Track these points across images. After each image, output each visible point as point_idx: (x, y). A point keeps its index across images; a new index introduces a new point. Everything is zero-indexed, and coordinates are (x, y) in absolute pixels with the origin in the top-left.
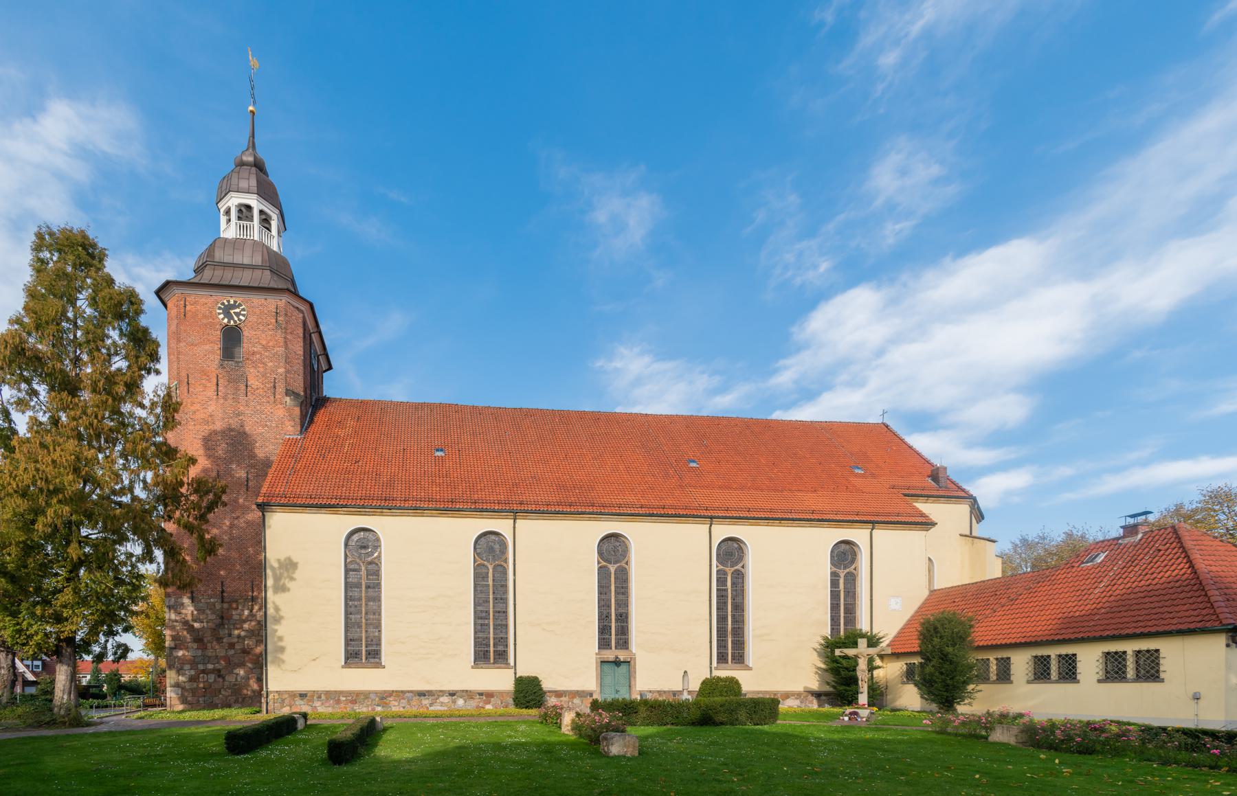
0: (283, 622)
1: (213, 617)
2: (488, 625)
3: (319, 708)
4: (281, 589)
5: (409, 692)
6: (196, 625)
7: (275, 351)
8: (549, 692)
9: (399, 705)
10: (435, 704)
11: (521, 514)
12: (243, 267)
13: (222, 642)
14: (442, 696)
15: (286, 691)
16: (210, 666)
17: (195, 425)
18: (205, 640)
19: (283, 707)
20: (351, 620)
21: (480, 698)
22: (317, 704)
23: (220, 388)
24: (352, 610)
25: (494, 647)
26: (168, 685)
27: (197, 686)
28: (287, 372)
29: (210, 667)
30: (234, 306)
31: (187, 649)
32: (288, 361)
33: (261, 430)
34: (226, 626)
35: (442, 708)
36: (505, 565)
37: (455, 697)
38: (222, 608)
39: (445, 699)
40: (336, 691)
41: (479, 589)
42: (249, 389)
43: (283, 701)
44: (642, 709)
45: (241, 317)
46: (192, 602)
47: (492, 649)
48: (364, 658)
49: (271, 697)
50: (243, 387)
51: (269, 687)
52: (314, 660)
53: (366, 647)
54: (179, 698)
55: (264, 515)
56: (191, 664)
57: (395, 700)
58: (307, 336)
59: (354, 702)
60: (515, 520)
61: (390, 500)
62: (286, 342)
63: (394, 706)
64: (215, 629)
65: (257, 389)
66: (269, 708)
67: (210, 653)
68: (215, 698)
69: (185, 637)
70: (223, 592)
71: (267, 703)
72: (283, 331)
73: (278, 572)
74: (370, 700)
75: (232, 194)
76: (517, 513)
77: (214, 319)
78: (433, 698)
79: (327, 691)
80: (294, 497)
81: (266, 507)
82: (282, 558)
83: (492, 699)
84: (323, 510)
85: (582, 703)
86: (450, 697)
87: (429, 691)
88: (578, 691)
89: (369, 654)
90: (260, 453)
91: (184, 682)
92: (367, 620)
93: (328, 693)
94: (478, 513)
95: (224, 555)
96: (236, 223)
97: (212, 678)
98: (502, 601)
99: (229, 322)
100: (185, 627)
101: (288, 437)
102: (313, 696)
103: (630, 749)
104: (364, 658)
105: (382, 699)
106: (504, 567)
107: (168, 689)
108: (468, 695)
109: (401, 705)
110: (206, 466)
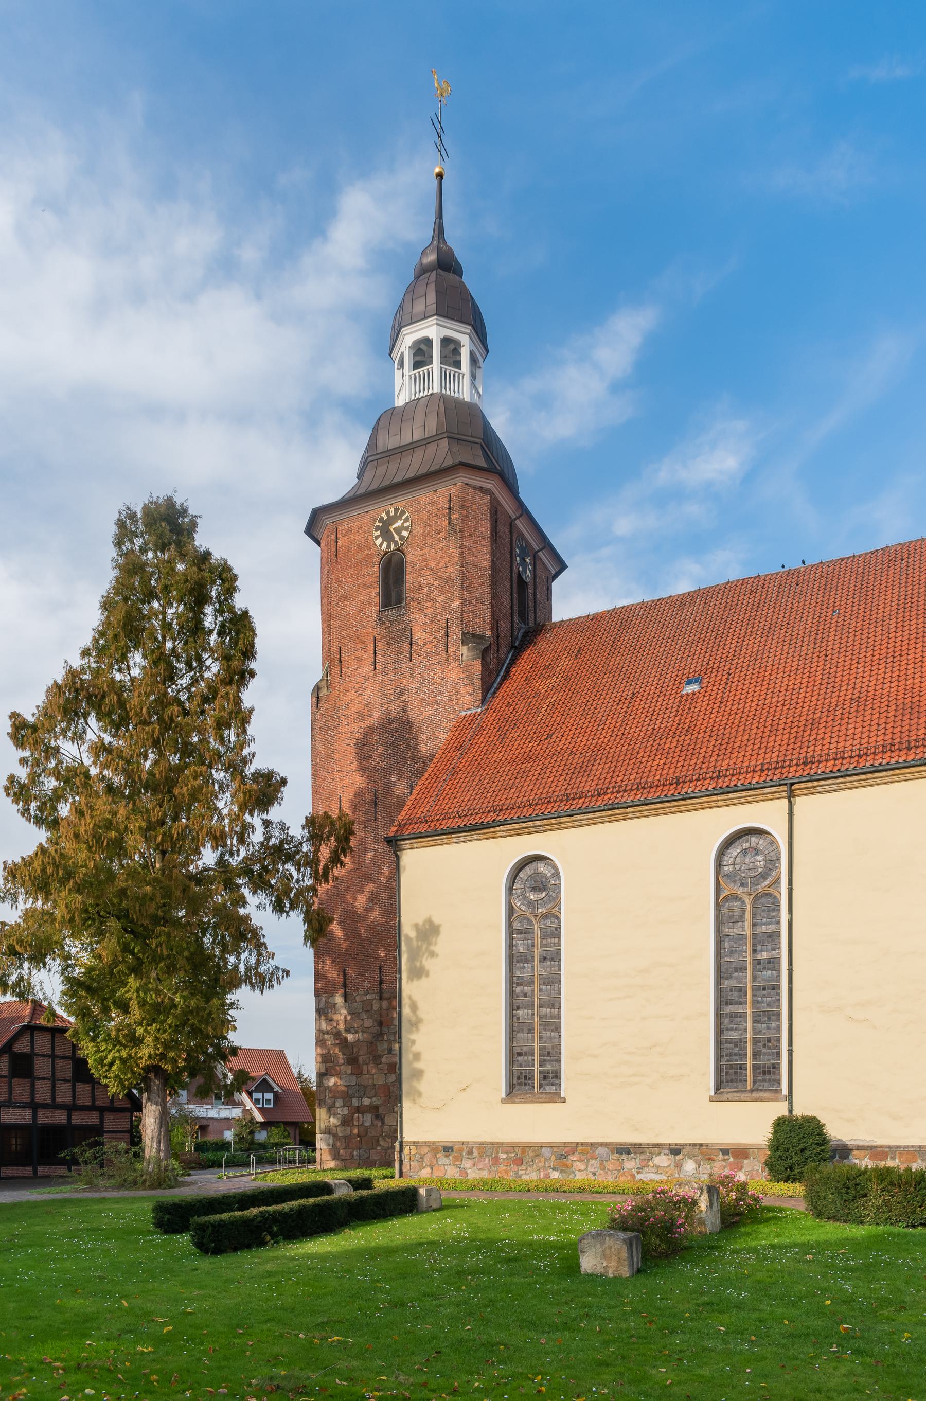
0: (422, 1028)
1: (368, 1023)
2: (743, 1015)
3: (469, 1171)
4: (418, 973)
5: (603, 1145)
6: (350, 1037)
7: (448, 574)
8: (859, 1148)
9: (586, 1169)
10: (646, 1169)
11: (802, 785)
12: (412, 447)
13: (381, 1063)
14: (659, 1154)
15: (426, 1142)
16: (366, 1102)
17: (348, 724)
18: (360, 1059)
19: (421, 1167)
20: (518, 1018)
21: (724, 1160)
22: (467, 1164)
24: (520, 1000)
25: (754, 1058)
26: (318, 1131)
27: (351, 1131)
29: (365, 1103)
30: (391, 520)
31: (338, 1074)
32: (466, 585)
33: (429, 711)
34: (385, 1037)
35: (657, 1177)
36: (776, 894)
37: (680, 1156)
38: (381, 1008)
39: (662, 1160)
40: (492, 1143)
41: (726, 945)
42: (414, 647)
43: (422, 1157)
44: (874, 1187)
45: (405, 534)
46: (345, 1001)
47: (749, 1062)
48: (536, 1085)
49: (406, 1151)
50: (406, 647)
51: (405, 1135)
52: (464, 1090)
53: (541, 1066)
54: (330, 1151)
56: (344, 1098)
57: (581, 1161)
58: (503, 530)
59: (519, 1162)
60: (791, 796)
62: (462, 553)
63: (579, 1170)
64: (372, 1043)
65: (425, 644)
66: (404, 1170)
67: (366, 1079)
68: (372, 1152)
69: (336, 1056)
70: (381, 982)
71: (401, 1161)
73: (415, 943)
74: (543, 1160)
75: (405, 331)
76: (792, 784)
77: (370, 550)
78: (643, 1157)
79: (481, 1143)
80: (875, 753)
82: (420, 922)
83: (746, 1162)
84: (475, 835)
86: (671, 1157)
87: (636, 1144)
89: (545, 1077)
90: (424, 749)
91: (336, 1126)
92: (541, 1018)
93: (482, 1146)
94: (720, 797)
95: (382, 924)
96: (441, 368)
97: (368, 1118)
98: (770, 966)
99: (389, 546)
100: (337, 1042)
101: (464, 714)
102: (461, 1151)
103: (613, 1264)
104: (536, 1085)
105: (561, 1157)
106: (775, 897)
107: (318, 1136)
108: (704, 1152)
109: (589, 1170)
110: (361, 786)
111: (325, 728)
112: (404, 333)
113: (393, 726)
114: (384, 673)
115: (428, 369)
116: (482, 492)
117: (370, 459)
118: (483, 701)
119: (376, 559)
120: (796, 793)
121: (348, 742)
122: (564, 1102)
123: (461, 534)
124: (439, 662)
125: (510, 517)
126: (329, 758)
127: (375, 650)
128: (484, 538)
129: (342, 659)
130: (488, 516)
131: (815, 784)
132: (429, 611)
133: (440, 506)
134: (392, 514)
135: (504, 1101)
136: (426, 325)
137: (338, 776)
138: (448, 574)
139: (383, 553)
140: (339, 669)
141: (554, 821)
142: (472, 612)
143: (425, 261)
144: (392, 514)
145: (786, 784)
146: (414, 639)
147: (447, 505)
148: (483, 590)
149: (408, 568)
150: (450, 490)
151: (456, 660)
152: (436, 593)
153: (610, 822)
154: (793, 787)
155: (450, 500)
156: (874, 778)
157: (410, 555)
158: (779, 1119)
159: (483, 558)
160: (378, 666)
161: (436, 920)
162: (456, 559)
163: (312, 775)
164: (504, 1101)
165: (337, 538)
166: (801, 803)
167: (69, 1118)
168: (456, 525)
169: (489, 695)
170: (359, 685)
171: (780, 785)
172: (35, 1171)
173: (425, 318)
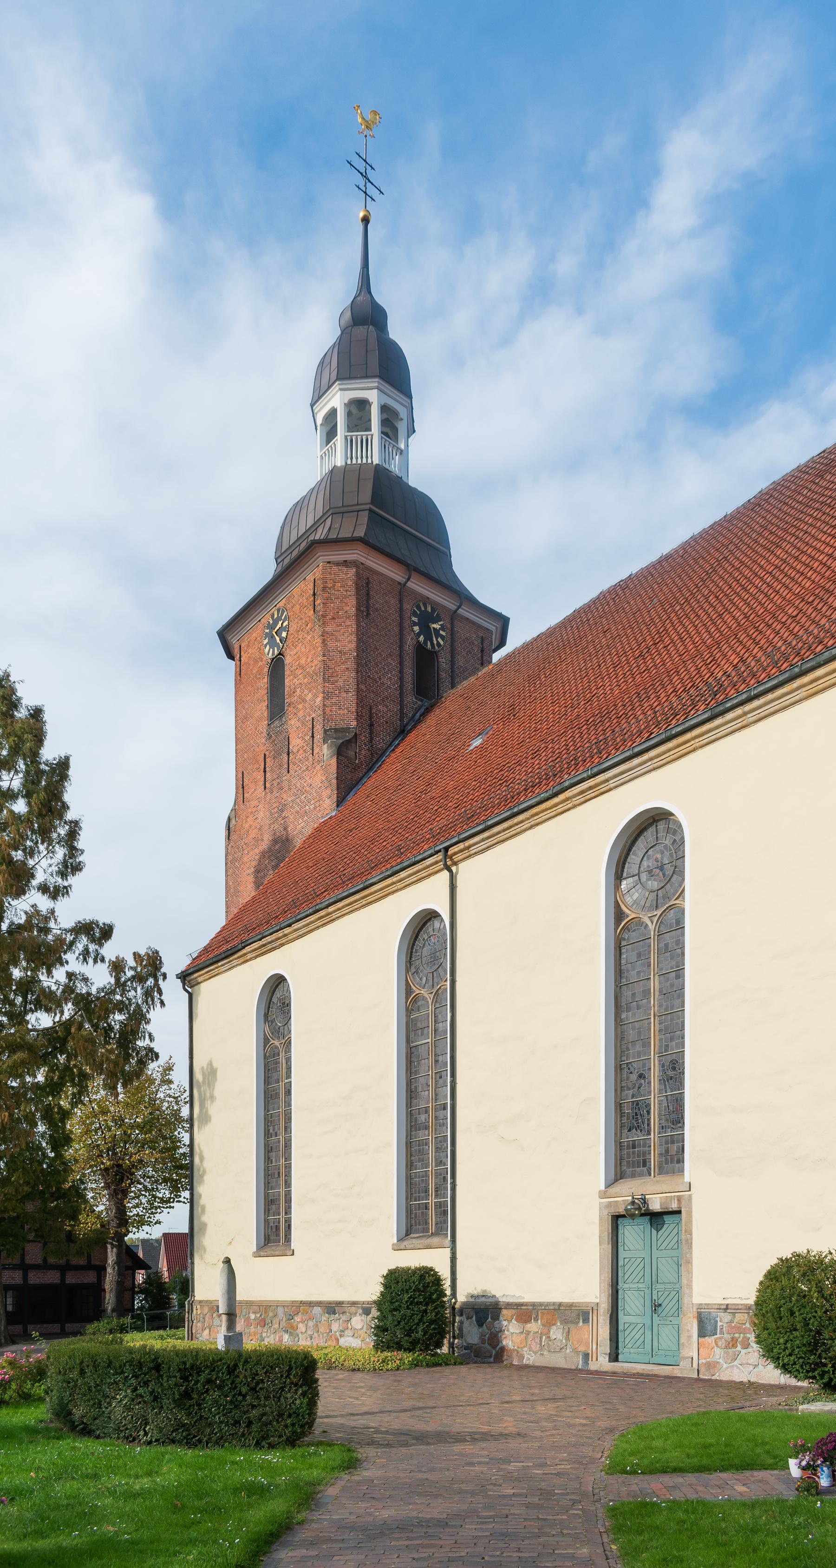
5: (319, 1304)
8: (509, 1306)
17: (248, 852)
23: (268, 775)
28: (327, 696)
32: (327, 674)
50: (285, 756)
62: (324, 641)
65: (298, 752)
76: (446, 849)
81: (188, 979)
85: (567, 1339)
88: (560, 1304)
96: (346, 437)
116: (347, 566)
117: (279, 560)
118: (339, 803)
119: (266, 670)
120: (456, 858)
122: (293, 1254)
123: (323, 619)
124: (307, 769)
125: (399, 583)
127: (265, 768)
128: (348, 618)
131: (467, 843)
132: (301, 714)
134: (276, 616)
135: (257, 1255)
136: (331, 395)
139: (270, 661)
141: (280, 934)
142: (335, 704)
144: (276, 616)
146: (291, 747)
147: (312, 593)
148: (347, 677)
149: (287, 673)
152: (306, 692)
154: (449, 853)
156: (516, 824)
158: (431, 1269)
159: (347, 641)
160: (268, 785)
161: (215, 1065)
164: (257, 1255)
165: (240, 657)
166: (466, 870)
167: (63, 1278)
172: (63, 1329)
173: (329, 387)
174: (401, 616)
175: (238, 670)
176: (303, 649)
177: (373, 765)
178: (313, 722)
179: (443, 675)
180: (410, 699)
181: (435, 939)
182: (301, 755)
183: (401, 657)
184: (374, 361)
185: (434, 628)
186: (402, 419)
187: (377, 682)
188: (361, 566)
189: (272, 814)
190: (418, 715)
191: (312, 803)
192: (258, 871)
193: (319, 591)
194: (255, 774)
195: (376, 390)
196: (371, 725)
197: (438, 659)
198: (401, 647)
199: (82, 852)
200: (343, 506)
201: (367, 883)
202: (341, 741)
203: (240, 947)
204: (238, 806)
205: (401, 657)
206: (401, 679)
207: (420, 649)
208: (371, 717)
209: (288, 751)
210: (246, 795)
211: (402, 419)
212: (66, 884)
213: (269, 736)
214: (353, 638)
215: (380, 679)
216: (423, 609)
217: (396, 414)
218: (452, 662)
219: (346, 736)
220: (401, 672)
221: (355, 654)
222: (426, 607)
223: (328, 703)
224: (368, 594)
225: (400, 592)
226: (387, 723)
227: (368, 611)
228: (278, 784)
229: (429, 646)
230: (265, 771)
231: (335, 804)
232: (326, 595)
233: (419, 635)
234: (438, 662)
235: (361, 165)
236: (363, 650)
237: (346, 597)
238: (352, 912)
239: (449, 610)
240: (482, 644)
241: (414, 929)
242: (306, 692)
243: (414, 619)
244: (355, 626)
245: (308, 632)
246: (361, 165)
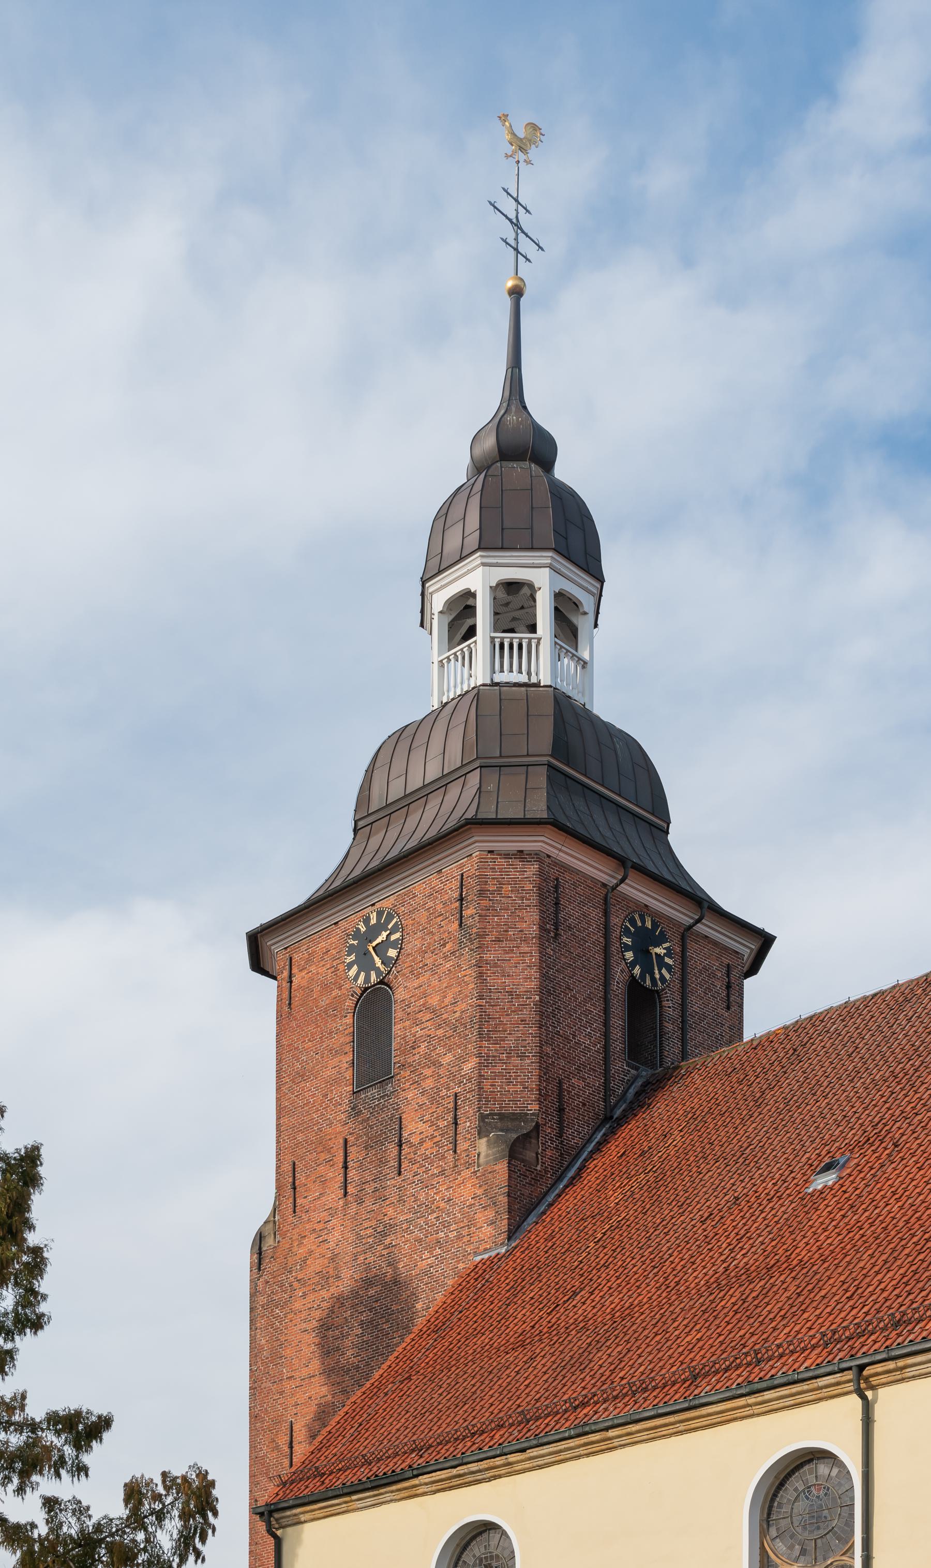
11: (879, 1368)
12: (425, 792)
17: (304, 1295)
28: (485, 1061)
42: (406, 1149)
55: (278, 1542)
61: (379, 1460)
62: (480, 975)
65: (422, 1142)
72: (476, 944)
76: (862, 1368)
77: (340, 988)
81: (276, 1515)
84: (387, 1493)
94: (751, 1400)
99: (367, 978)
101: (478, 1258)
111: (271, 1304)
112: (431, 590)
113: (372, 1292)
114: (360, 1201)
115: (462, 650)
116: (522, 860)
117: (361, 824)
119: (349, 1003)
120: (874, 1381)
121: (304, 1325)
123: (480, 941)
124: (442, 1172)
125: (604, 885)
126: (276, 1357)
127: (345, 1162)
129: (297, 1183)
130: (534, 899)
131: (901, 1363)
132: (429, 1084)
133: (446, 897)
134: (373, 921)
137: (288, 1386)
138: (458, 1014)
139: (359, 992)
140: (291, 1200)
141: (499, 1461)
142: (501, 1075)
143: (478, 451)
144: (373, 921)
145: (850, 1369)
147: (456, 895)
149: (397, 1012)
150: (462, 866)
151: (468, 1165)
152: (440, 1050)
153: (588, 1455)
154: (865, 1373)
155: (462, 885)
157: (401, 989)
160: (350, 1189)
162: (472, 986)
163: (251, 1388)
165: (290, 976)
168: (471, 927)
169: (532, 1218)
170: (321, 1226)
171: (842, 1370)
173: (462, 559)
174: (606, 936)
175: (286, 995)
176: (435, 982)
177: (563, 1173)
178: (456, 1100)
179: (669, 1027)
180: (619, 1065)
181: (819, 1490)
182: (428, 1148)
183: (606, 1000)
184: (546, 525)
185: (656, 953)
186: (585, 613)
187: (569, 1041)
188: (547, 860)
189: (359, 1237)
190: (632, 1091)
191: (452, 1228)
192: (325, 1327)
193: (471, 895)
194: (321, 1168)
195: (548, 569)
196: (561, 1110)
197: (660, 1002)
198: (606, 985)
199: (44, 1297)
200: (501, 756)
201: (697, 1402)
202: (515, 1136)
203: (409, 1474)
204: (282, 1217)
205: (606, 1000)
206: (606, 1035)
207: (634, 985)
208: (560, 1096)
209: (400, 1141)
210: (299, 1201)
211: (585, 613)
212: (9, 1346)
213: (355, 1111)
214: (534, 973)
215: (574, 1036)
216: (639, 924)
217: (576, 605)
218: (683, 1006)
219: (522, 1128)
220: (606, 1024)
221: (537, 998)
222: (643, 922)
223: (488, 1072)
224: (557, 904)
225: (606, 899)
226: (584, 1105)
227: (557, 929)
228: (376, 1190)
229: (648, 982)
230: (346, 1167)
231: (505, 1236)
232: (485, 903)
233: (633, 964)
234: (661, 1007)
235: (509, 207)
236: (549, 992)
237: (520, 908)
238: (653, 1439)
239: (677, 924)
240: (728, 976)
241: (779, 1474)
242: (440, 1050)
243: (625, 940)
244: (535, 954)
245: (446, 957)
246: (509, 207)
